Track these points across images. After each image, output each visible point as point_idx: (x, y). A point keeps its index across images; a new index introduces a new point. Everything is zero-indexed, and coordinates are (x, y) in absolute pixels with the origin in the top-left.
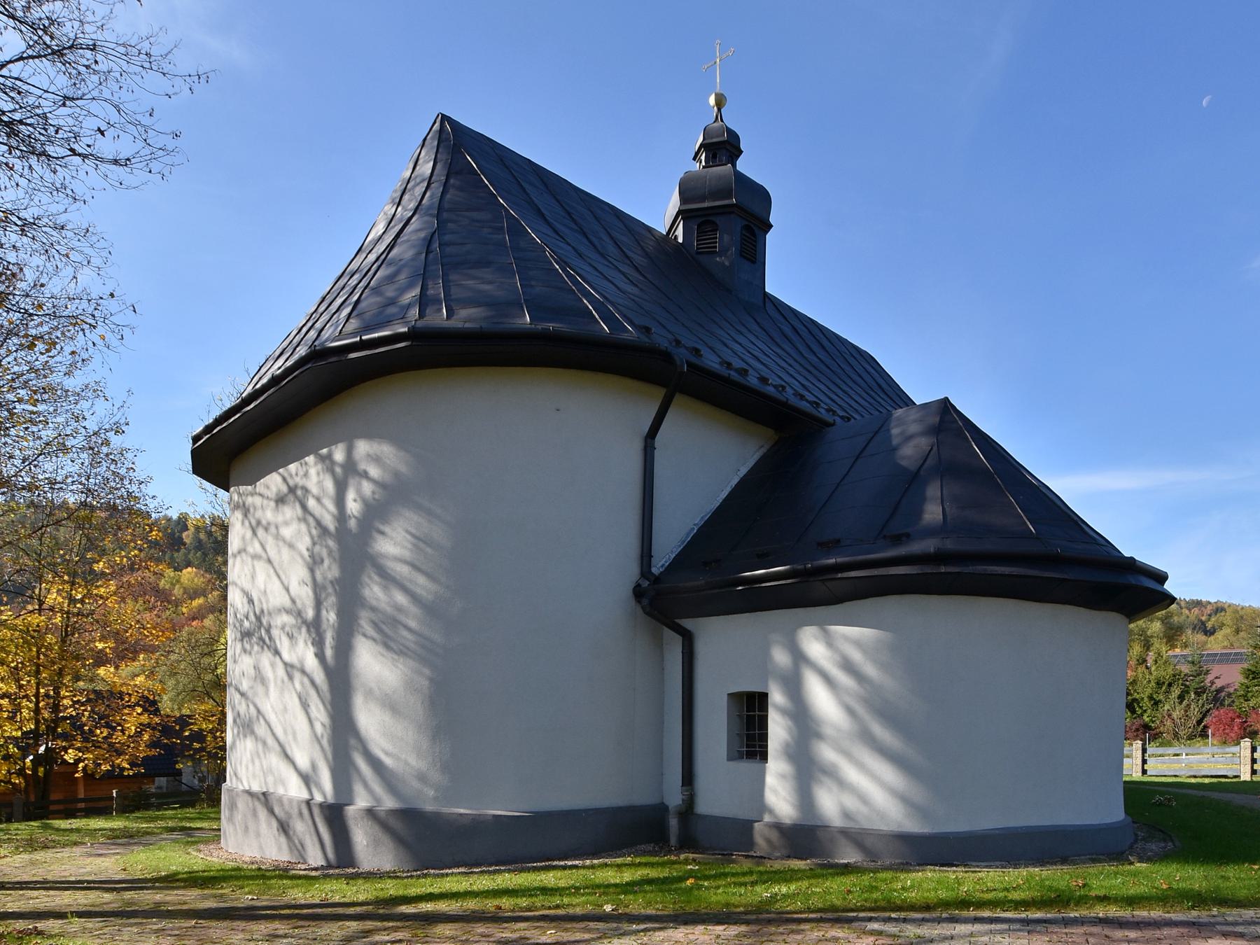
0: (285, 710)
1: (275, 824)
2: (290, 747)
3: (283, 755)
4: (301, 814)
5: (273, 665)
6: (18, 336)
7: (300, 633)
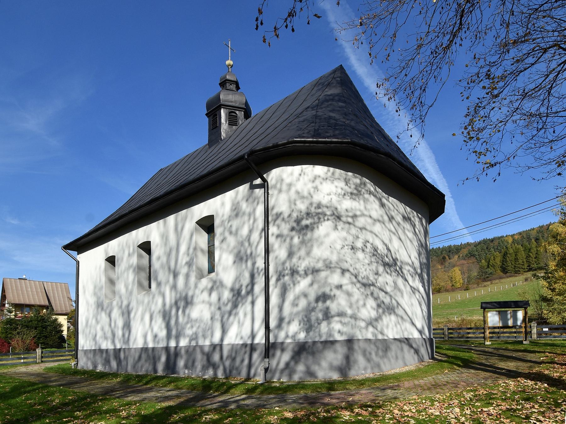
0: (412, 304)
1: (412, 351)
2: (415, 320)
3: (411, 323)
4: (423, 345)
5: (404, 285)
6: (330, 268)
7: (416, 277)
